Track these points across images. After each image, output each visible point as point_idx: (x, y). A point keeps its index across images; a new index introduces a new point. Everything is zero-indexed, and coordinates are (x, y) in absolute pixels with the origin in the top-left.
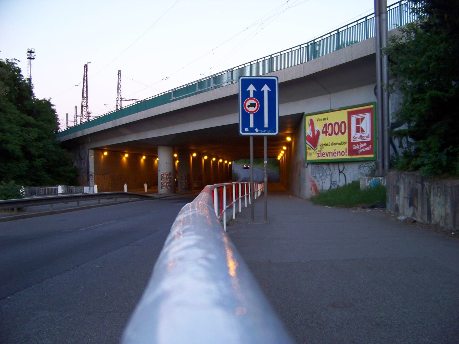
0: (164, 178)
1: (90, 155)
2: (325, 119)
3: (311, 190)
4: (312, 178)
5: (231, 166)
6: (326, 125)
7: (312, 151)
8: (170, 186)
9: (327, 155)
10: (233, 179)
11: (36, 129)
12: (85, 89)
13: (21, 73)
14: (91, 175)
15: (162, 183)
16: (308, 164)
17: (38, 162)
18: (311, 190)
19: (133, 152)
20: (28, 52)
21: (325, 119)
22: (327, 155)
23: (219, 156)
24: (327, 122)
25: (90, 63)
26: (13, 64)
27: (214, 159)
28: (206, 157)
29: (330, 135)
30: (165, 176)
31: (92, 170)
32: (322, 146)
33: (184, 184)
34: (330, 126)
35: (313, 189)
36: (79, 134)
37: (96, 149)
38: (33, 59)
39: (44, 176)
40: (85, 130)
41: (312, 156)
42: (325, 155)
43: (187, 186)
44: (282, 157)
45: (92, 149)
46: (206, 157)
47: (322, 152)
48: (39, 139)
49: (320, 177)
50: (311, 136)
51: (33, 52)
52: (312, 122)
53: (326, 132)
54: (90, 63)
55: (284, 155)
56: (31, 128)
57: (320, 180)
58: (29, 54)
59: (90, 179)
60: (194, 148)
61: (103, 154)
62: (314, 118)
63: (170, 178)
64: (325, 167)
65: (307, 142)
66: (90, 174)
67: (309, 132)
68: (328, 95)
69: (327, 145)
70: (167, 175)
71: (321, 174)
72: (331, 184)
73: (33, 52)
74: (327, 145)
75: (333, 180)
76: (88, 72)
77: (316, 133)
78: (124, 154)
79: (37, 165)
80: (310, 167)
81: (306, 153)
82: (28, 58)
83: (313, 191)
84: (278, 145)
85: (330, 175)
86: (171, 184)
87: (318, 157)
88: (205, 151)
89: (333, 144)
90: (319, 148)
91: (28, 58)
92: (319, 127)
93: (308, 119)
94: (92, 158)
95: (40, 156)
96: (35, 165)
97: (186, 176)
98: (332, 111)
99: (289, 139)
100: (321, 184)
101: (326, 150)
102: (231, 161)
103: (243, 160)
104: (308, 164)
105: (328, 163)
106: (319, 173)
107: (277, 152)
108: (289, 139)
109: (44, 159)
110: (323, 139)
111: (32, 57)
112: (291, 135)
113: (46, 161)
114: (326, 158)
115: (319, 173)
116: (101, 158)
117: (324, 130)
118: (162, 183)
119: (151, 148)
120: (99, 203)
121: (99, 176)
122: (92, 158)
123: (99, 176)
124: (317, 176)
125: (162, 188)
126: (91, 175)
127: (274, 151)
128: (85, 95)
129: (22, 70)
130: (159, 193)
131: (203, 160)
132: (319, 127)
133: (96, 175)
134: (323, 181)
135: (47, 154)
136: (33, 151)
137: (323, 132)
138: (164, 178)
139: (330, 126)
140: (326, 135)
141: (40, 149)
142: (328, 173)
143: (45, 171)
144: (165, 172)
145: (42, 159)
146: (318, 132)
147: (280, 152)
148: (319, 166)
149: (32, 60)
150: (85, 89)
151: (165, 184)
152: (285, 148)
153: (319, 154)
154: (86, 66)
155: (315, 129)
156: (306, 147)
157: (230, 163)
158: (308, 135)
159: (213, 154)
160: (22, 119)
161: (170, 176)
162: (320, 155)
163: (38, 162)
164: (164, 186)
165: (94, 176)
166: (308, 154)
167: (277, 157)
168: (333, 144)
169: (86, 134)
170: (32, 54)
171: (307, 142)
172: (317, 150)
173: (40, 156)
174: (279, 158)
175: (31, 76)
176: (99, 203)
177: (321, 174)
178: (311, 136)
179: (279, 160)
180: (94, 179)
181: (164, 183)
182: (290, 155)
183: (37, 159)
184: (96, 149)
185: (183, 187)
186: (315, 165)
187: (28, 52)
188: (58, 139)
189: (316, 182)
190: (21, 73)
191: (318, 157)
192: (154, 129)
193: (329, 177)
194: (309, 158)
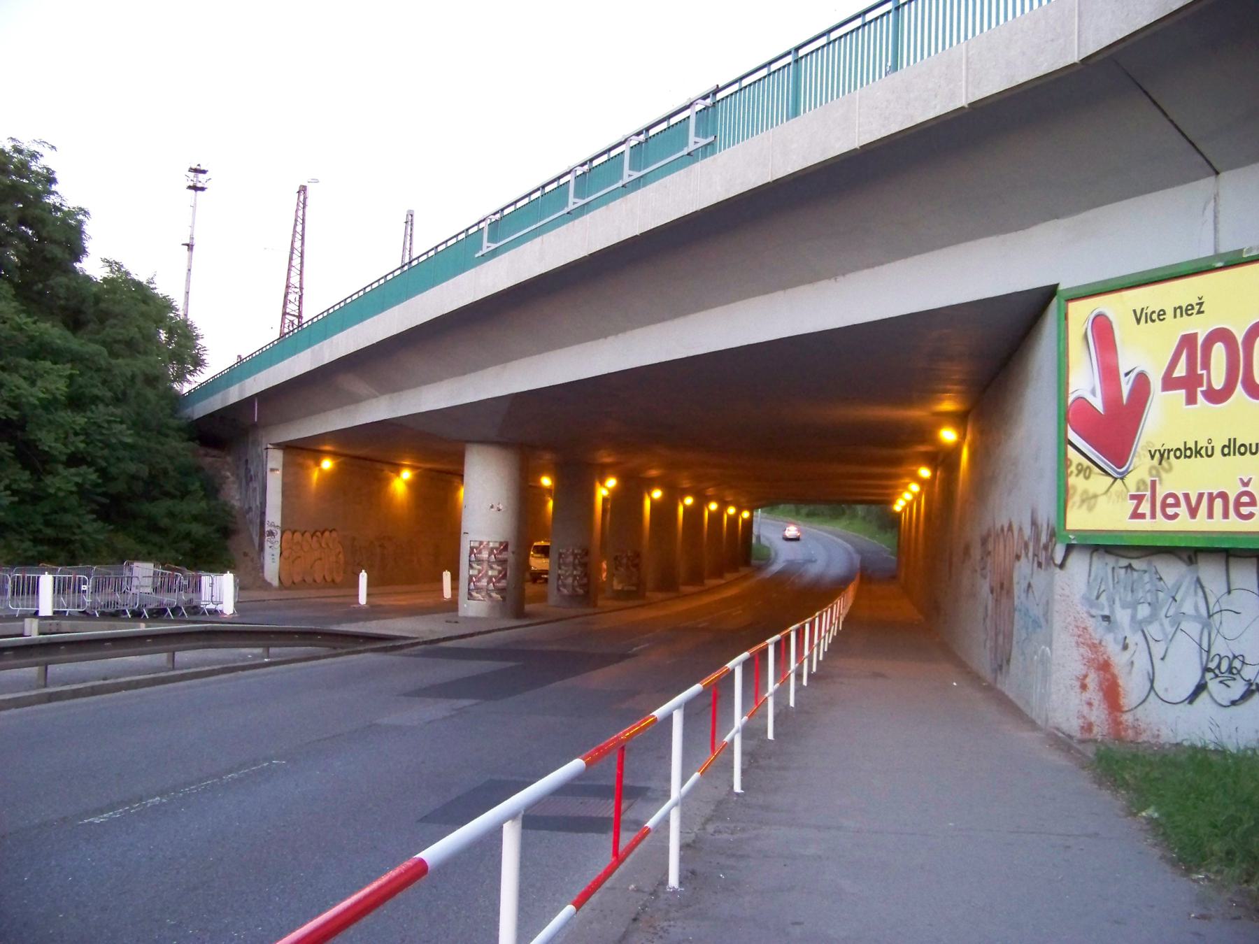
0: (479, 561)
1: (270, 465)
2: (1184, 311)
3: (1084, 687)
4: (1090, 623)
5: (748, 524)
6: (1188, 341)
7: (1099, 482)
8: (501, 591)
9: (1193, 512)
10: (754, 562)
11: (67, 369)
12: (296, 261)
13: (54, 188)
14: (271, 533)
15: (471, 577)
16: (1069, 548)
17: (63, 481)
18: (1084, 687)
19: (429, 466)
20: (192, 170)
21: (1184, 311)
22: (1193, 512)
23: (710, 491)
24: (1201, 327)
25: (317, 181)
26: (34, 155)
27: (713, 506)
28: (689, 501)
29: (1216, 397)
30: (485, 555)
31: (274, 515)
32: (1162, 455)
33: (570, 580)
34: (1219, 351)
35: (1093, 680)
36: (234, 395)
37: (290, 448)
38: (202, 189)
39: (88, 528)
40: (249, 381)
41: (1100, 506)
42: (1183, 510)
43: (580, 591)
44: (910, 504)
45: (278, 446)
46: (689, 501)
47: (1161, 492)
48: (76, 401)
49: (1139, 626)
50: (1098, 403)
51: (204, 172)
52: (1102, 330)
53: (1190, 385)
54: (317, 181)
55: (917, 498)
56: (48, 364)
57: (1135, 639)
58: (192, 175)
59: (267, 545)
60: (608, 460)
61: (318, 464)
62: (1117, 307)
63: (502, 562)
64: (1172, 572)
65: (1073, 436)
66: (267, 528)
67: (1084, 382)
68: (1206, 185)
69: (1194, 452)
70: (491, 552)
71: (1143, 611)
72: (1206, 670)
73: (204, 172)
74: (1194, 452)
75: (1219, 647)
76: (307, 209)
77: (1126, 387)
78: (397, 468)
79: (59, 489)
80: (1078, 564)
81: (1063, 495)
82: (190, 187)
83: (1094, 693)
84: (898, 461)
85: (1197, 617)
86: (503, 584)
87: (1136, 515)
88: (654, 473)
89: (1232, 448)
90: (1140, 466)
91: (190, 187)
92: (1146, 351)
93: (1080, 314)
94: (274, 483)
95: (75, 460)
96: (52, 491)
97: (575, 556)
98: (1235, 261)
99: (948, 435)
100: (1142, 661)
101: (1186, 478)
102: (751, 510)
103: (792, 507)
104: (1069, 548)
105: (1191, 553)
106: (1134, 606)
107: (896, 487)
108: (948, 435)
109: (91, 470)
110: (1166, 418)
111: (199, 185)
112: (959, 420)
113: (94, 477)
114: (1183, 523)
115: (1134, 606)
116: (309, 477)
117: (1181, 371)
118: (471, 577)
119: (439, 446)
120: (45, 680)
121: (298, 536)
122: (274, 483)
123: (298, 536)
124: (1122, 616)
125: (470, 597)
126: (271, 533)
127: (885, 483)
128: (295, 280)
129: (57, 176)
130: (461, 613)
131: (681, 510)
132: (1146, 351)
133: (288, 535)
134: (1158, 650)
135: (106, 452)
136: (47, 440)
137: (1170, 383)
138: (479, 561)
139: (1219, 351)
140: (1191, 400)
141: (76, 434)
142: (1188, 608)
143: (92, 512)
144: (485, 539)
145: (84, 469)
146: (1142, 382)
147: (905, 487)
148: (1136, 564)
149: (199, 192)
150: (296, 261)
151: (484, 582)
152: (925, 472)
153: (1139, 498)
154: (303, 189)
155: (1123, 368)
156: (1064, 462)
157: (746, 514)
158: (1080, 399)
159: (686, 484)
160: (21, 329)
161: (503, 556)
162: (1145, 508)
163: (63, 481)
164: (478, 589)
165: (278, 537)
166: (1074, 500)
167: (892, 502)
168: (1232, 448)
169: (248, 394)
170: (201, 176)
171: (1073, 436)
172: (1131, 480)
173: (75, 460)
174: (898, 506)
175: (192, 238)
176: (45, 680)
177: (1143, 611)
178: (1098, 403)
179: (899, 515)
180: (277, 546)
181: (479, 580)
182: (943, 501)
183: (60, 468)
184: (290, 448)
185: (565, 591)
186: (1111, 560)
187: (192, 170)
188: (188, 412)
189: (1112, 648)
190: (54, 188)
191: (1136, 515)
192: (441, 379)
193: (1193, 628)
194: (1078, 520)
